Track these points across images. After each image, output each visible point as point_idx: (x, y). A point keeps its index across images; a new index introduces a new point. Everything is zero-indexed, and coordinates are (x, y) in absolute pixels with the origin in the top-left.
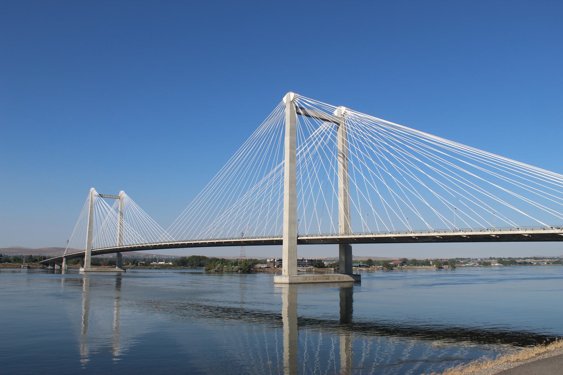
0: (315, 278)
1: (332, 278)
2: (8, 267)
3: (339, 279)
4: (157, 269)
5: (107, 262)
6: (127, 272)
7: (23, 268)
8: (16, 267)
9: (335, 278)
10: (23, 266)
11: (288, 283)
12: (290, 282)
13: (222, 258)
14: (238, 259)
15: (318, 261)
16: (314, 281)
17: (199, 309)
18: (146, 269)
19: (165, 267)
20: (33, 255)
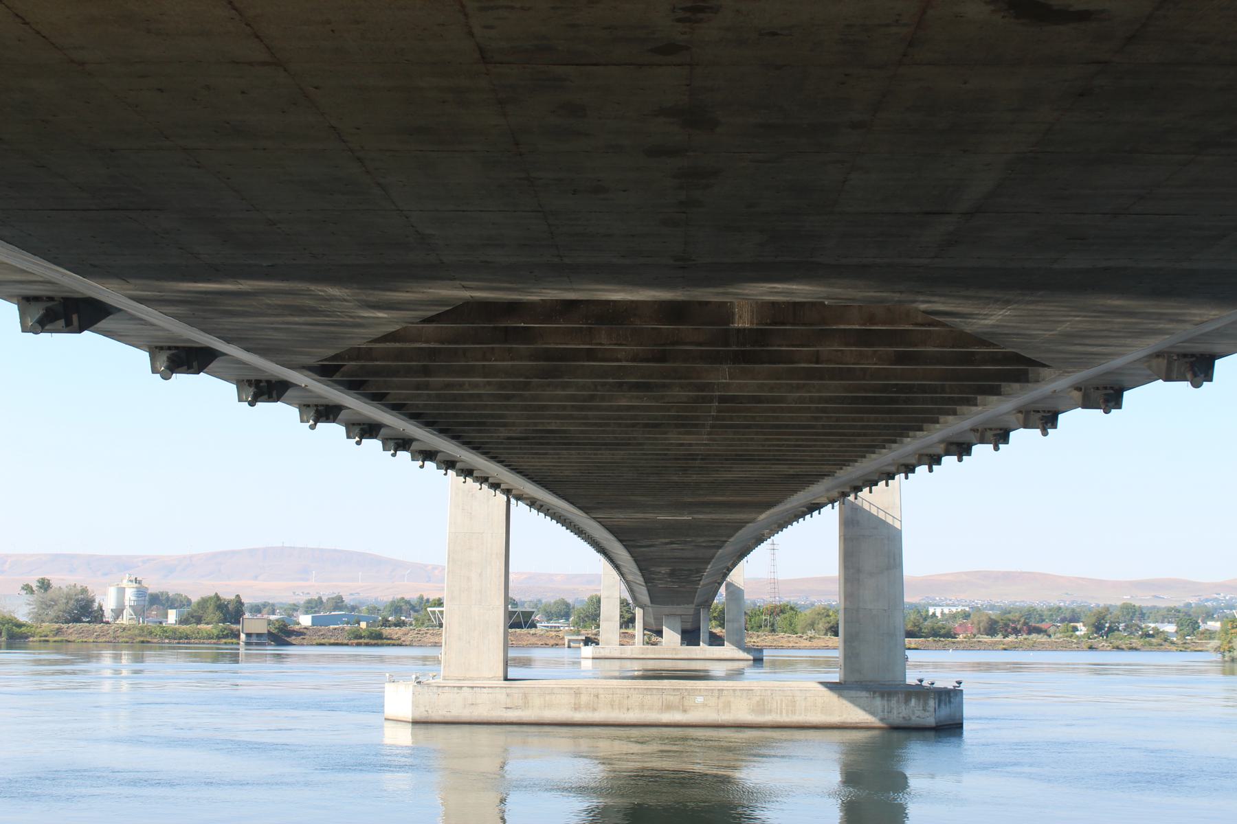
0: (584, 699)
1: (705, 705)
2: (525, 643)
3: (761, 707)
4: (1122, 649)
5: (979, 623)
6: (589, 658)
7: (569, 647)
8: (552, 642)
9: (728, 705)
10: (570, 641)
11: (411, 720)
12: (421, 714)
13: (558, 597)
14: (1107, 609)
15: (256, 606)
16: (578, 717)
17: (39, 791)
18: (1072, 650)
19: (1166, 640)
20: (1136, 605)
